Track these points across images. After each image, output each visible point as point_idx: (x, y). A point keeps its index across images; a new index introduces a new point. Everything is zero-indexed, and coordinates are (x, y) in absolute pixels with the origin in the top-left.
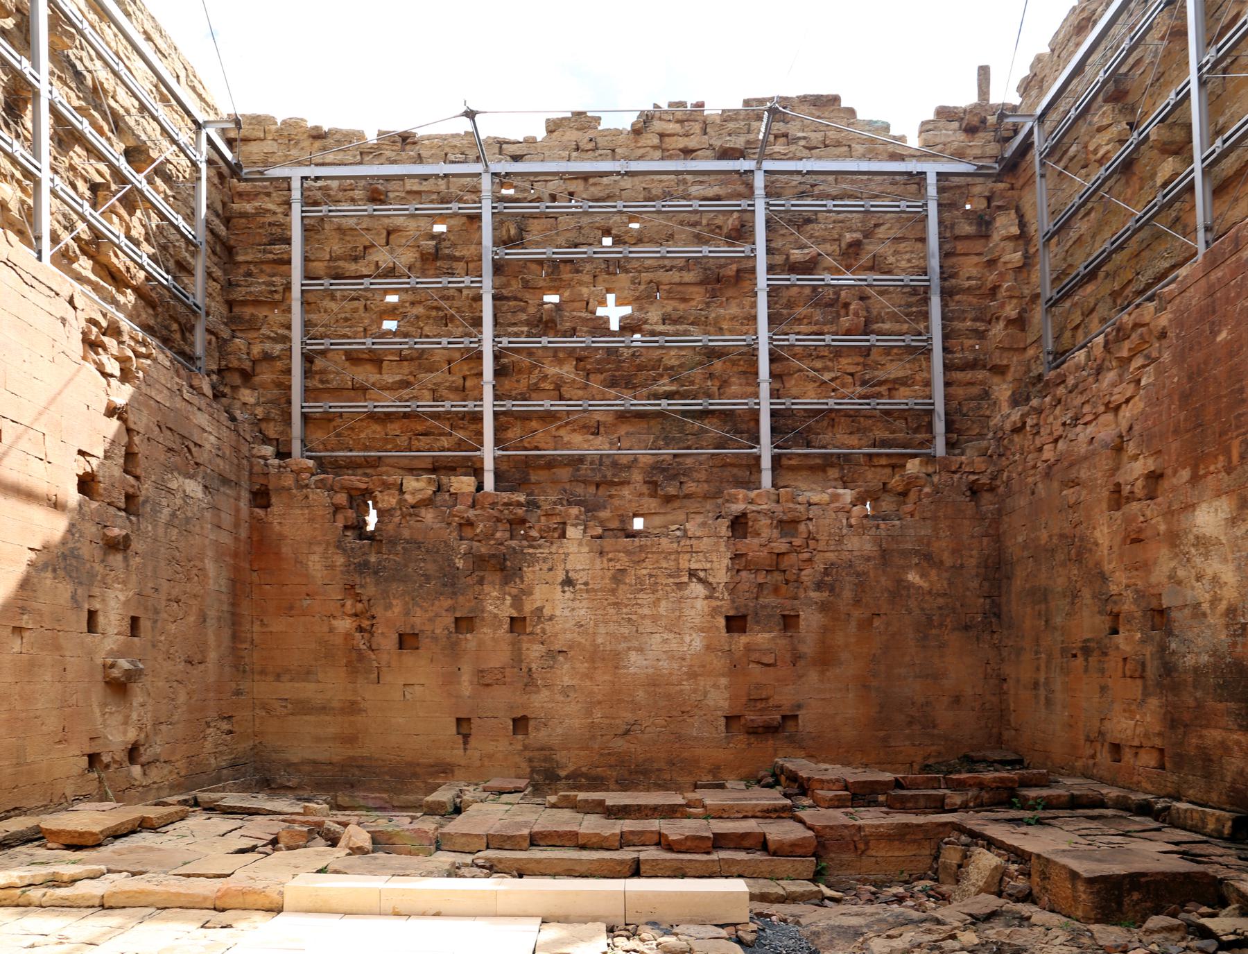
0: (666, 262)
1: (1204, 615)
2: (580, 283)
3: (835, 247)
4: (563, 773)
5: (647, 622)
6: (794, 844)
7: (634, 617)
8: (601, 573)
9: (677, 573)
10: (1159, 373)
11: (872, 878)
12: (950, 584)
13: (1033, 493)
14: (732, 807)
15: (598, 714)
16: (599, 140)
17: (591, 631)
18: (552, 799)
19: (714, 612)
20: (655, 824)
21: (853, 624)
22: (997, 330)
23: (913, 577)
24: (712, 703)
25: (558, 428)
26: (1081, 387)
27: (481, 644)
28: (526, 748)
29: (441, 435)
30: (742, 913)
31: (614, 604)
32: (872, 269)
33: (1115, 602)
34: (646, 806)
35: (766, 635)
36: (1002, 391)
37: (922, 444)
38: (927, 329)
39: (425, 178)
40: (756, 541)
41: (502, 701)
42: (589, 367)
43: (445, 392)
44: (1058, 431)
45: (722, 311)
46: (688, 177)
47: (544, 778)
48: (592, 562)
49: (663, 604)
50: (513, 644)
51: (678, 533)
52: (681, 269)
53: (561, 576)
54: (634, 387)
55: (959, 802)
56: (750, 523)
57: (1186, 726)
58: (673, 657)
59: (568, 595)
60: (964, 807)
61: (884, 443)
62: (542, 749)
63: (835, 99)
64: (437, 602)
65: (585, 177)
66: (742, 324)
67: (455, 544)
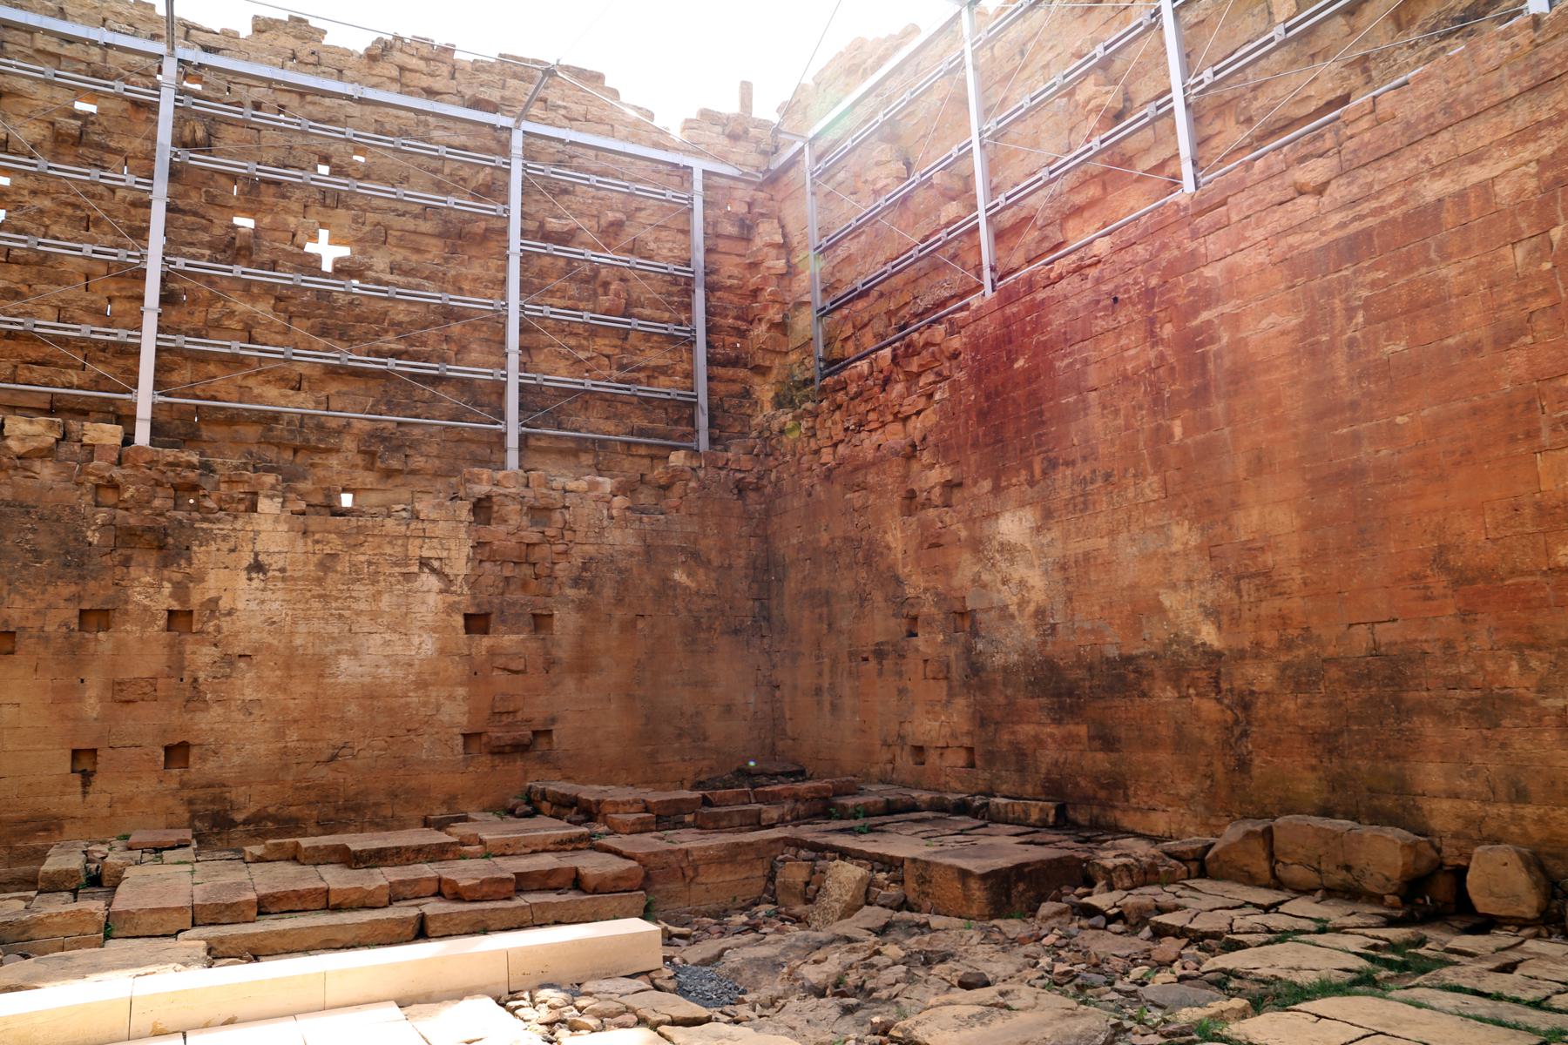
0: (399, 206)
1: (1012, 617)
2: (287, 211)
3: (594, 223)
4: (239, 817)
5: (364, 619)
6: (618, 878)
7: (347, 613)
8: (303, 557)
9: (405, 561)
10: (955, 387)
11: (703, 908)
12: (719, 584)
13: (810, 495)
14: (518, 841)
15: (293, 736)
16: (323, 55)
17: (287, 629)
18: (257, 850)
19: (451, 608)
20: (428, 870)
21: (615, 625)
22: (760, 330)
23: (679, 576)
24: (446, 718)
25: (246, 377)
26: (866, 395)
27: (119, 647)
28: (183, 785)
29: (68, 367)
30: (653, 957)
31: (320, 596)
32: (631, 251)
33: (912, 605)
34: (407, 848)
35: (514, 637)
36: (765, 391)
37: (683, 436)
38: (690, 320)
39: (70, 40)
40: (503, 528)
41: (149, 724)
42: (292, 309)
43: (78, 313)
44: (838, 433)
45: (464, 270)
46: (431, 119)
47: (214, 826)
48: (292, 543)
49: (386, 598)
50: (171, 646)
51: (404, 514)
52: (416, 217)
53: (248, 559)
54: (351, 340)
55: (775, 816)
56: (496, 508)
57: (997, 723)
58: (397, 663)
59: (255, 583)
60: (782, 821)
61: (642, 432)
62: (210, 786)
63: (597, 78)
64: (51, 589)
65: (302, 92)
66: (486, 287)
67: (88, 511)
